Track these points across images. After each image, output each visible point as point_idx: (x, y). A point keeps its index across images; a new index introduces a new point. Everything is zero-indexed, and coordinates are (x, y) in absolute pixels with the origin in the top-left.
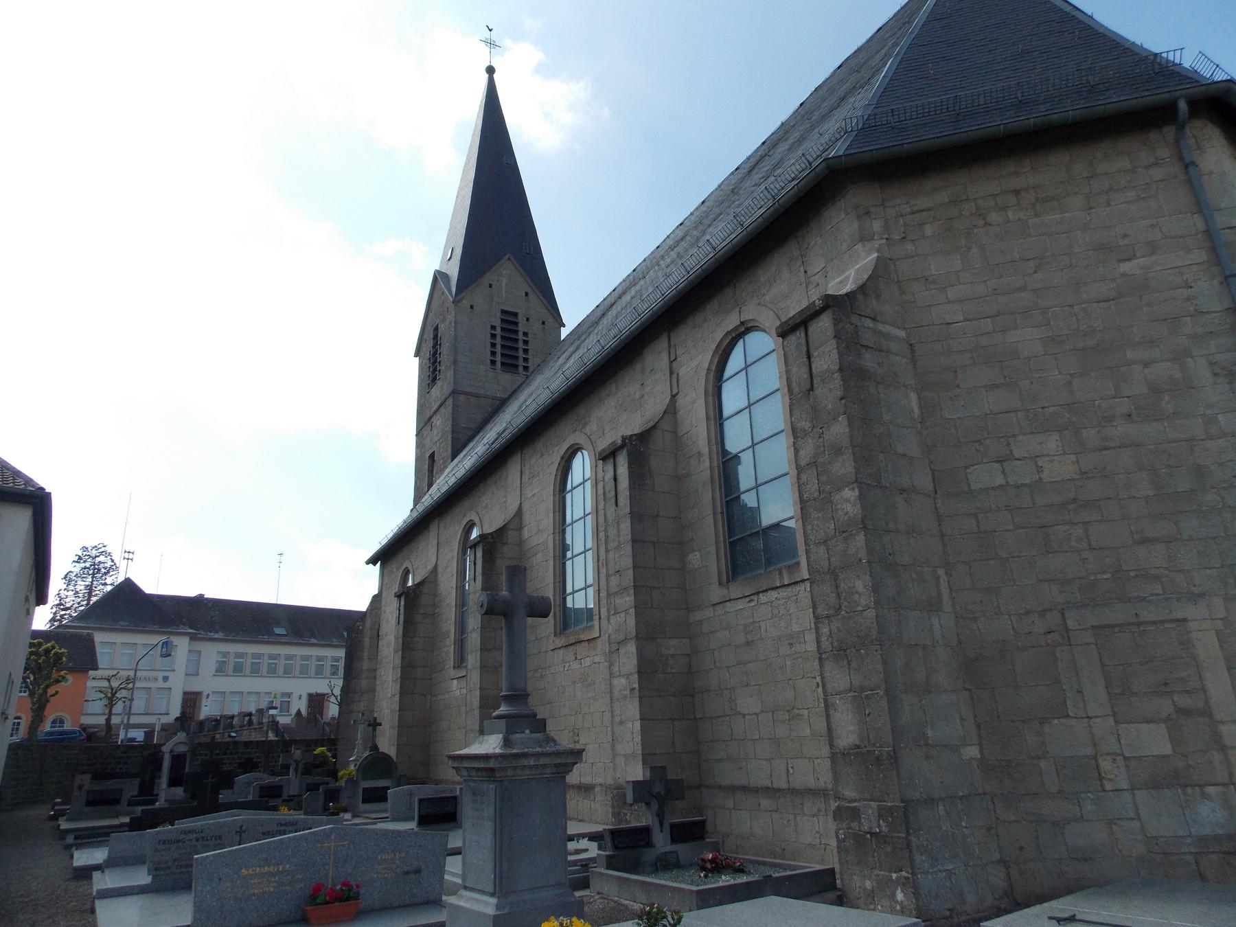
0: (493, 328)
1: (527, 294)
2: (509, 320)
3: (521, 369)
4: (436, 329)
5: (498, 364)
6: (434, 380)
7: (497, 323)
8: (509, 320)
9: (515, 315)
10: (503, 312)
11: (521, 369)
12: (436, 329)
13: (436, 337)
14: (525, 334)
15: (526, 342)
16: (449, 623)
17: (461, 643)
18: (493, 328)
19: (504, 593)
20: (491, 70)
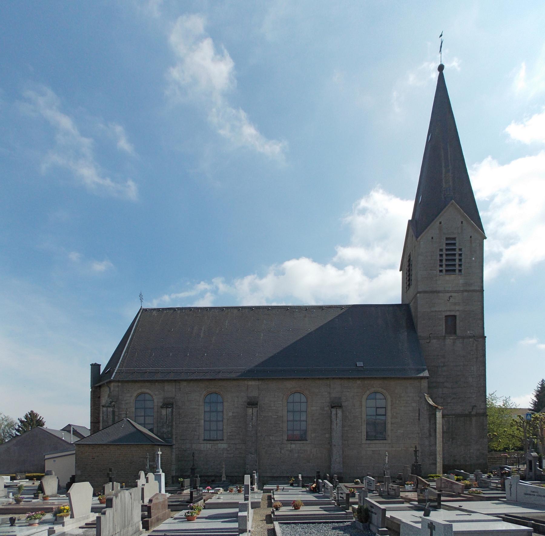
0: (441, 250)
1: (462, 222)
2: (451, 243)
3: (457, 271)
4: (410, 256)
5: (444, 271)
6: (409, 285)
7: (444, 247)
8: (451, 243)
9: (454, 239)
10: (447, 239)
11: (457, 271)
12: (410, 256)
13: (409, 260)
14: (460, 250)
15: (460, 265)
16: (218, 524)
17: (337, 522)
18: (441, 250)
19: (160, 453)
20: (441, 68)
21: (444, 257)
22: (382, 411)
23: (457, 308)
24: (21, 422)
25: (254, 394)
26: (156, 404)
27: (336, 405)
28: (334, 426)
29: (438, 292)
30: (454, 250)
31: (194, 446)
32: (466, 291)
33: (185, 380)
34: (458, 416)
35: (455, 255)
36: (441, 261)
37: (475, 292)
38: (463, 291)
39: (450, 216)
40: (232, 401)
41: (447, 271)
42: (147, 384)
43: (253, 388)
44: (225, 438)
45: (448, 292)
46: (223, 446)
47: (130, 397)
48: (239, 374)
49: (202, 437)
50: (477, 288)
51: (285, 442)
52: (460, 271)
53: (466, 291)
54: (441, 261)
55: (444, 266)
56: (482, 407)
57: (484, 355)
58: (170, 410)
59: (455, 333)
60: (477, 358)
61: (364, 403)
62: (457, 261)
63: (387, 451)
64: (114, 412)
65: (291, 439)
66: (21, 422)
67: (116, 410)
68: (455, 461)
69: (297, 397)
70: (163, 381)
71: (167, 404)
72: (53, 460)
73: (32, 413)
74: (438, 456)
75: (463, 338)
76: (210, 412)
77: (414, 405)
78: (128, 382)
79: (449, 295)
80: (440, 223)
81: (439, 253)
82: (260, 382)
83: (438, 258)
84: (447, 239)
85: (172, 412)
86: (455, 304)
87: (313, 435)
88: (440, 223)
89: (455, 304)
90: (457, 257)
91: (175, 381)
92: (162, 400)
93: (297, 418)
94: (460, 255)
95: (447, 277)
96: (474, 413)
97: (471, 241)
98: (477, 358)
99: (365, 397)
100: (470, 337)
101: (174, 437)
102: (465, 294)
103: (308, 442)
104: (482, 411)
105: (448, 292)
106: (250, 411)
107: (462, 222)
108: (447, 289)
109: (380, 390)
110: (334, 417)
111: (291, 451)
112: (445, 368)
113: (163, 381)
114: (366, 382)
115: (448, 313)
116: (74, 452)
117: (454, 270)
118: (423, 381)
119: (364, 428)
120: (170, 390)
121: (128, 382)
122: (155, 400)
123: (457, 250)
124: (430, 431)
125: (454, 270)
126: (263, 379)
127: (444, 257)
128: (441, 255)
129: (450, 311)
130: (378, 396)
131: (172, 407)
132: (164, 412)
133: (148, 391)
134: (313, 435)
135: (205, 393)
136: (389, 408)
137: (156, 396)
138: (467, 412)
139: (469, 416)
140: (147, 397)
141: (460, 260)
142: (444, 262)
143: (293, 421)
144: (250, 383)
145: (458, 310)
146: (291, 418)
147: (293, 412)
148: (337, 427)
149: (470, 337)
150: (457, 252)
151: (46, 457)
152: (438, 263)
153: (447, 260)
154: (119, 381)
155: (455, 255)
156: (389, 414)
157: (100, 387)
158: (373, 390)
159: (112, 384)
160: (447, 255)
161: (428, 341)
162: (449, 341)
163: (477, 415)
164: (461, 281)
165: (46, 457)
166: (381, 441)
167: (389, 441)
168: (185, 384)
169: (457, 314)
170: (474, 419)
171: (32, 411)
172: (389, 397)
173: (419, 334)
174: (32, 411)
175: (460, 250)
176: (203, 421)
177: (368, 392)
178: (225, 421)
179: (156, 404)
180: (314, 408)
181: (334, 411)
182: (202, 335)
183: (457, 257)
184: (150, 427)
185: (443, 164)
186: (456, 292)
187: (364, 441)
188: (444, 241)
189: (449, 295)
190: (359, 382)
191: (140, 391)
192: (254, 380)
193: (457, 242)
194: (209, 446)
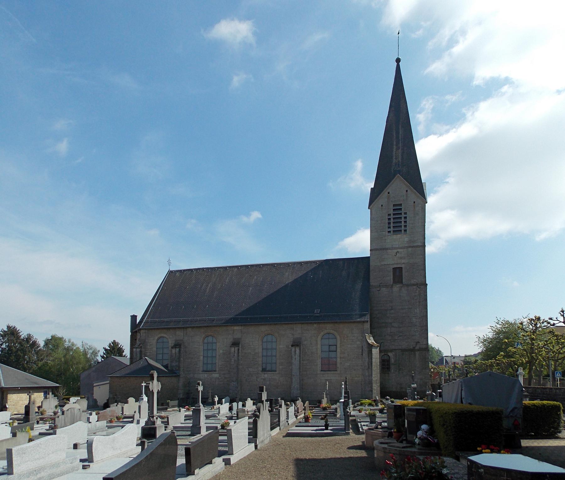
1: (407, 191)
2: (397, 208)
3: (403, 231)
5: (392, 232)
7: (392, 212)
8: (397, 208)
10: (394, 205)
11: (403, 231)
14: (405, 213)
18: (389, 215)
21: (392, 220)
22: (333, 348)
23: (403, 261)
24: (106, 350)
25: (238, 336)
26: (170, 345)
27: (296, 344)
28: (293, 361)
29: (387, 249)
30: (401, 214)
31: (196, 376)
32: (410, 247)
33: (190, 327)
34: (404, 350)
35: (401, 218)
36: (389, 223)
37: (419, 247)
38: (408, 247)
39: (398, 186)
40: (222, 341)
41: (394, 231)
42: (164, 330)
43: (237, 331)
44: (217, 370)
45: (395, 248)
46: (216, 375)
47: (152, 341)
48: (223, 322)
49: (201, 369)
50: (420, 244)
51: (260, 372)
52: (405, 231)
53: (410, 247)
54: (389, 223)
55: (392, 228)
56: (425, 343)
57: (426, 300)
58: (178, 349)
59: (401, 282)
60: (420, 302)
61: (319, 342)
62: (403, 222)
63: (327, 380)
64: (141, 351)
65: (264, 370)
66: (106, 350)
67: (143, 350)
68: (402, 388)
69: (270, 338)
70: (175, 328)
71: (177, 345)
72: (98, 387)
73: (114, 342)
74: (374, 385)
75: (408, 285)
76: (208, 350)
77: (358, 343)
78: (152, 329)
79: (396, 251)
80: (389, 193)
81: (387, 217)
82: (243, 327)
83: (387, 221)
84: (394, 205)
85: (180, 351)
86: (401, 258)
87: (281, 367)
88: (389, 193)
89: (401, 258)
90: (403, 220)
91: (183, 328)
92: (174, 342)
93: (269, 354)
94: (405, 218)
95: (395, 237)
96: (417, 348)
97: (414, 206)
98: (420, 302)
99: (320, 337)
100: (414, 285)
101: (182, 369)
102: (410, 249)
103: (277, 372)
104: (424, 346)
105: (395, 248)
106: (233, 349)
107: (407, 191)
108: (394, 246)
109: (332, 331)
110: (293, 353)
111: (264, 379)
112: (392, 311)
113: (175, 328)
114: (321, 325)
115: (396, 266)
116: (108, 382)
117: (401, 231)
118: (365, 324)
119: (319, 362)
120: (180, 334)
121: (152, 329)
122: (170, 342)
123: (403, 214)
124: (368, 364)
125: (401, 231)
126: (244, 325)
127: (392, 220)
128: (389, 219)
129: (397, 264)
130: (331, 336)
131: (180, 347)
132: (174, 351)
133: (165, 335)
134: (281, 367)
135: (204, 336)
136: (338, 345)
137: (170, 338)
138: (411, 347)
139: (413, 350)
140: (165, 340)
141: (405, 222)
142: (392, 225)
143: (267, 356)
144: (235, 328)
145: (403, 263)
146: (265, 354)
147: (267, 349)
148: (296, 361)
149: (414, 285)
150: (403, 215)
151: (95, 385)
152: (387, 225)
153: (394, 222)
154: (145, 329)
155: (401, 218)
156: (338, 350)
157: (136, 332)
158: (326, 331)
159: (142, 331)
160: (394, 218)
161: (379, 289)
162: (396, 288)
163: (420, 350)
164: (406, 239)
165: (95, 385)
166: (332, 372)
167: (338, 372)
168: (190, 329)
169: (403, 266)
170: (417, 353)
171: (114, 341)
172: (338, 337)
173: (371, 284)
174: (114, 341)
175: (405, 213)
176: (202, 357)
177: (322, 333)
178: (217, 356)
179: (170, 345)
180: (281, 346)
181: (293, 349)
182: (208, 290)
183: (403, 220)
184: (165, 363)
185: (395, 143)
186: (401, 248)
187: (319, 372)
188: (392, 208)
189: (396, 251)
190: (315, 325)
191: (159, 336)
192: (238, 325)
193: (403, 207)
194: (206, 375)
